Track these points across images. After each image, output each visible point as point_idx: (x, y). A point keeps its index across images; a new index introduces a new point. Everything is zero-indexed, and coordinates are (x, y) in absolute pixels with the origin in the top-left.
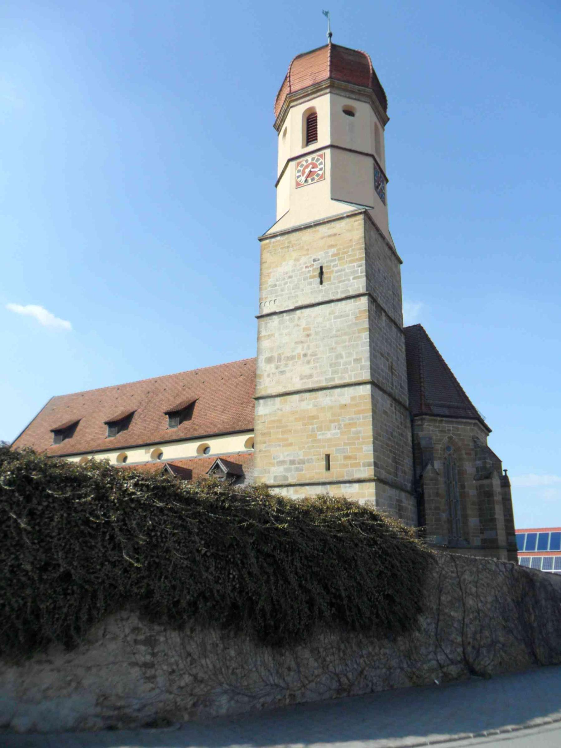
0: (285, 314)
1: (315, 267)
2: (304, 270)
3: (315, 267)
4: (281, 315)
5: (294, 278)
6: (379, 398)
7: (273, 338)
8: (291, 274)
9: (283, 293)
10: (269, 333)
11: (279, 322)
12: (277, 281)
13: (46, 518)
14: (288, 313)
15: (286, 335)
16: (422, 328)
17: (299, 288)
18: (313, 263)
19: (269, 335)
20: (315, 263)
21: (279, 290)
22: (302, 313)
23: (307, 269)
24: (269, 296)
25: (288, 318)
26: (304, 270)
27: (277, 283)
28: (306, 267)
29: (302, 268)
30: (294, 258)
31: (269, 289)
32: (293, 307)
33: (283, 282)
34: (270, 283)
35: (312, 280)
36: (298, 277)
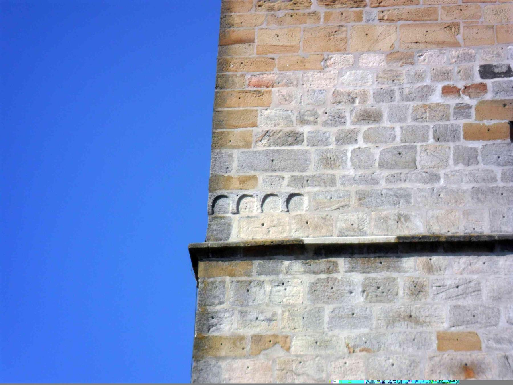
0: (342, 262)
1: (489, 96)
2: (436, 98)
3: (489, 96)
4: (323, 263)
5: (386, 123)
6: (258, 329)
7: (278, 353)
8: (370, 104)
9: (338, 173)
10: (260, 329)
11: (313, 290)
12: (303, 122)
13: (435, 287)
14: (359, 261)
15: (351, 350)
16: (194, 346)
17: (413, 164)
18: (478, 80)
19: (257, 339)
20: (489, 82)
21: (314, 157)
22: (430, 269)
23: (452, 101)
24: (261, 177)
25: (357, 278)
26: (436, 98)
27: (306, 130)
28: (447, 91)
29: (428, 90)
30: (385, 45)
31: (262, 147)
32: (391, 238)
33: (333, 131)
34: (263, 127)
35: (478, 145)
36: (410, 122)
